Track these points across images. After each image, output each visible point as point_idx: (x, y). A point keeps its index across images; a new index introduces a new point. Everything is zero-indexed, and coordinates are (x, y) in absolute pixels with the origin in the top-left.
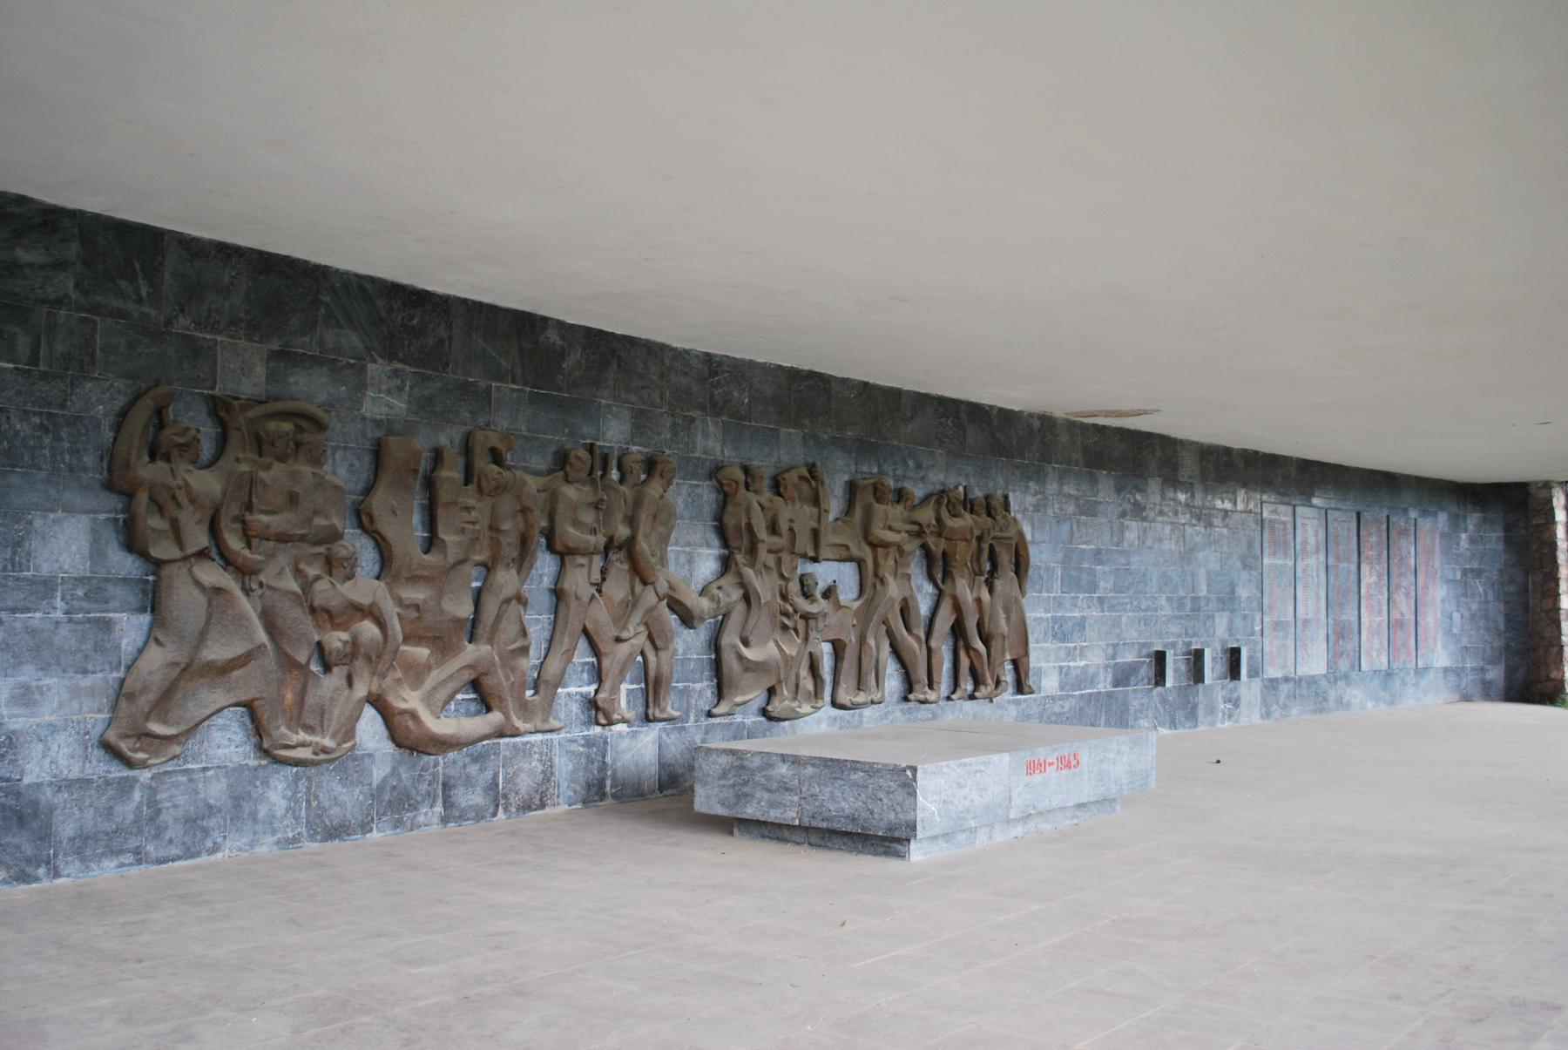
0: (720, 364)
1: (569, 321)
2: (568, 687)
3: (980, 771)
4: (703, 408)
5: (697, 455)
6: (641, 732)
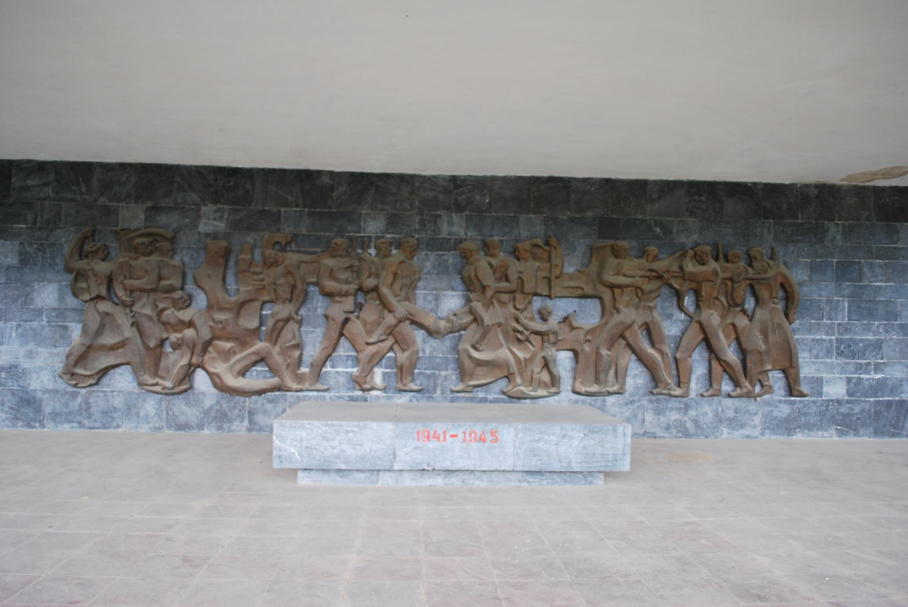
4: (448, 209)
5: (443, 236)
6: (395, 397)
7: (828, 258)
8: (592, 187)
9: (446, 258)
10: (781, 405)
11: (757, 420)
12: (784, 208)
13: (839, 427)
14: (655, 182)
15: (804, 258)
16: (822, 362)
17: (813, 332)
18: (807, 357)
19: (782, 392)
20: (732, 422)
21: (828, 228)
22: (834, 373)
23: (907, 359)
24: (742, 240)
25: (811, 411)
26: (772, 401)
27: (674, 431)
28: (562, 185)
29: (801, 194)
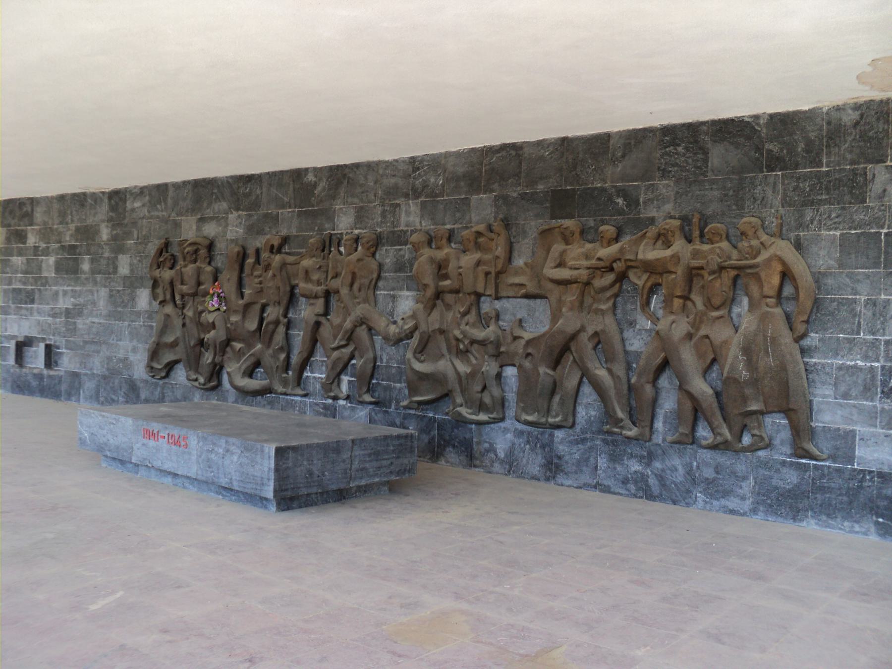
0: (422, 161)
1: (319, 166)
2: (314, 373)
3: (113, 424)
4: (406, 196)
5: (401, 228)
6: (358, 408)
7: (872, 228)
8: (546, 152)
9: (402, 253)
10: (784, 470)
11: (747, 487)
12: (799, 149)
13: (881, 520)
14: (620, 133)
15: (830, 230)
16: (854, 406)
17: (842, 353)
18: (829, 396)
19: (787, 450)
20: (711, 486)
21: (874, 175)
22: (876, 426)
23: (1, 364)
24: (734, 207)
25: (833, 485)
26: (771, 462)
27: (632, 487)
28: (513, 153)
29: (829, 123)
